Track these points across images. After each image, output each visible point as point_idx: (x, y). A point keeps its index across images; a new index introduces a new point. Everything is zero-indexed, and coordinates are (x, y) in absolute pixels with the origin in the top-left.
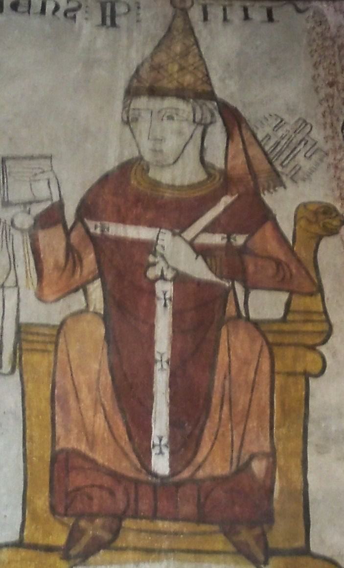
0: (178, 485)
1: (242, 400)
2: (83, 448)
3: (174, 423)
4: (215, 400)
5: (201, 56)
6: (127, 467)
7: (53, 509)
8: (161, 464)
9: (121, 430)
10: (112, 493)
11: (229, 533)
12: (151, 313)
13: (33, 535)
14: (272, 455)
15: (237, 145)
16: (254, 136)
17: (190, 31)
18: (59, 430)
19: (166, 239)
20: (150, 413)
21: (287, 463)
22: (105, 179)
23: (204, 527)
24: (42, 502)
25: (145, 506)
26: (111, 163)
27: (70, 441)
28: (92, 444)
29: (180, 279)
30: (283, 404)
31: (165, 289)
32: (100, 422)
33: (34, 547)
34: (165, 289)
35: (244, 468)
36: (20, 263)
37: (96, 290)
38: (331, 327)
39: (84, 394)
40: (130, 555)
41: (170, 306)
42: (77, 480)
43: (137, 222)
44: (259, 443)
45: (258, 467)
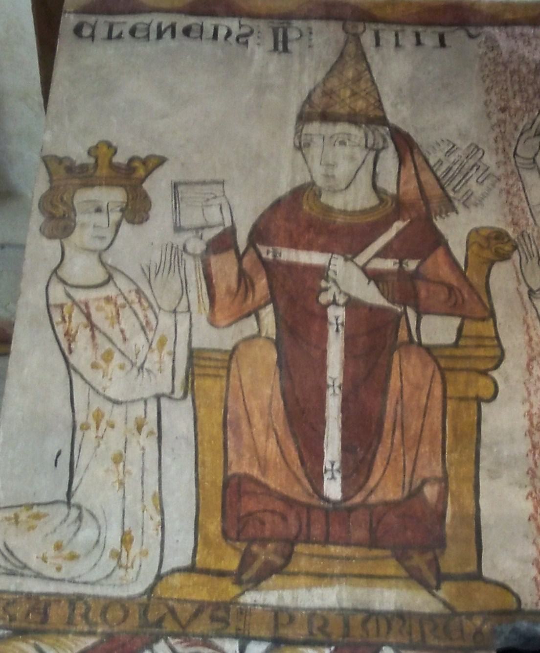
0: (350, 510)
1: (414, 425)
2: (255, 472)
3: (346, 448)
4: (388, 425)
5: (373, 82)
6: (299, 492)
7: (225, 534)
8: (333, 489)
9: (293, 455)
10: (284, 518)
11: (401, 558)
12: (323, 338)
13: (206, 560)
14: (444, 480)
16: (427, 161)
17: (362, 56)
18: (232, 455)
19: (338, 265)
20: (322, 438)
21: (459, 488)
22: (277, 204)
23: (376, 552)
24: (214, 527)
25: (317, 531)
26: (283, 188)
27: (242, 466)
28: (264, 470)
29: (352, 305)
30: (455, 429)
31: (337, 314)
33: (206, 572)
34: (337, 314)
35: (416, 493)
36: (192, 288)
37: (268, 315)
38: (503, 352)
39: (256, 419)
40: (302, 580)
41: (342, 330)
42: (250, 505)
43: (309, 247)
44: (431, 468)
45: (430, 492)
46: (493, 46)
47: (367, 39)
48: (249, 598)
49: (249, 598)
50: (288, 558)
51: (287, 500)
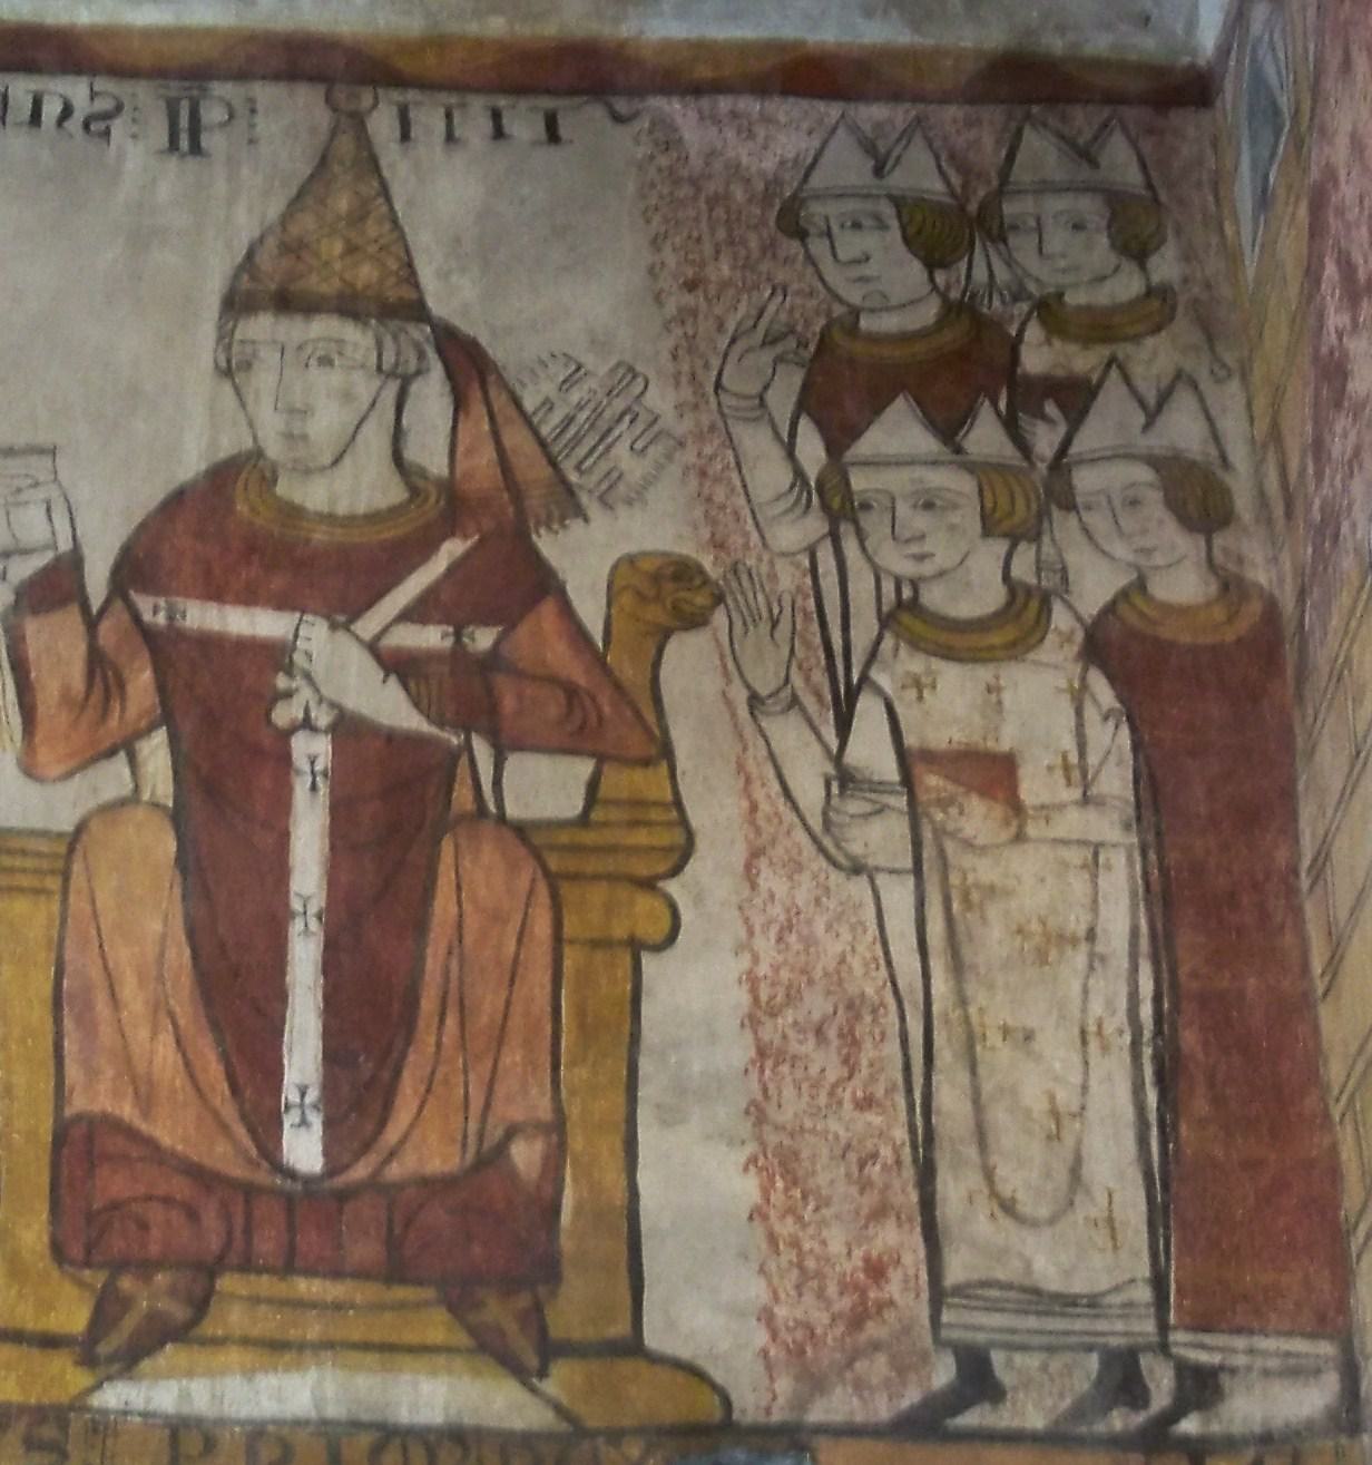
0: (343, 1196)
1: (488, 1003)
2: (127, 1111)
3: (335, 1056)
4: (428, 1004)
5: (395, 222)
6: (226, 1155)
7: (58, 1251)
8: (304, 1149)
9: (213, 1071)
11: (459, 1304)
15: (477, 424)
16: (517, 403)
17: (370, 163)
18: (73, 1072)
19: (316, 639)
20: (279, 1033)
21: (591, 1145)
22: (177, 500)
23: (401, 1293)
25: (267, 1243)
26: (191, 464)
29: (348, 729)
30: (581, 1013)
31: (312, 751)
32: (165, 1054)
34: (312, 751)
35: (492, 1158)
37: (156, 753)
38: (690, 837)
39: (129, 989)
40: (234, 1355)
41: (323, 788)
43: (249, 597)
44: (528, 1100)
45: (526, 1156)
46: (669, 141)
47: (382, 125)
48: (114, 1396)
49: (114, 1396)
50: (201, 1305)
51: (203, 1177)
